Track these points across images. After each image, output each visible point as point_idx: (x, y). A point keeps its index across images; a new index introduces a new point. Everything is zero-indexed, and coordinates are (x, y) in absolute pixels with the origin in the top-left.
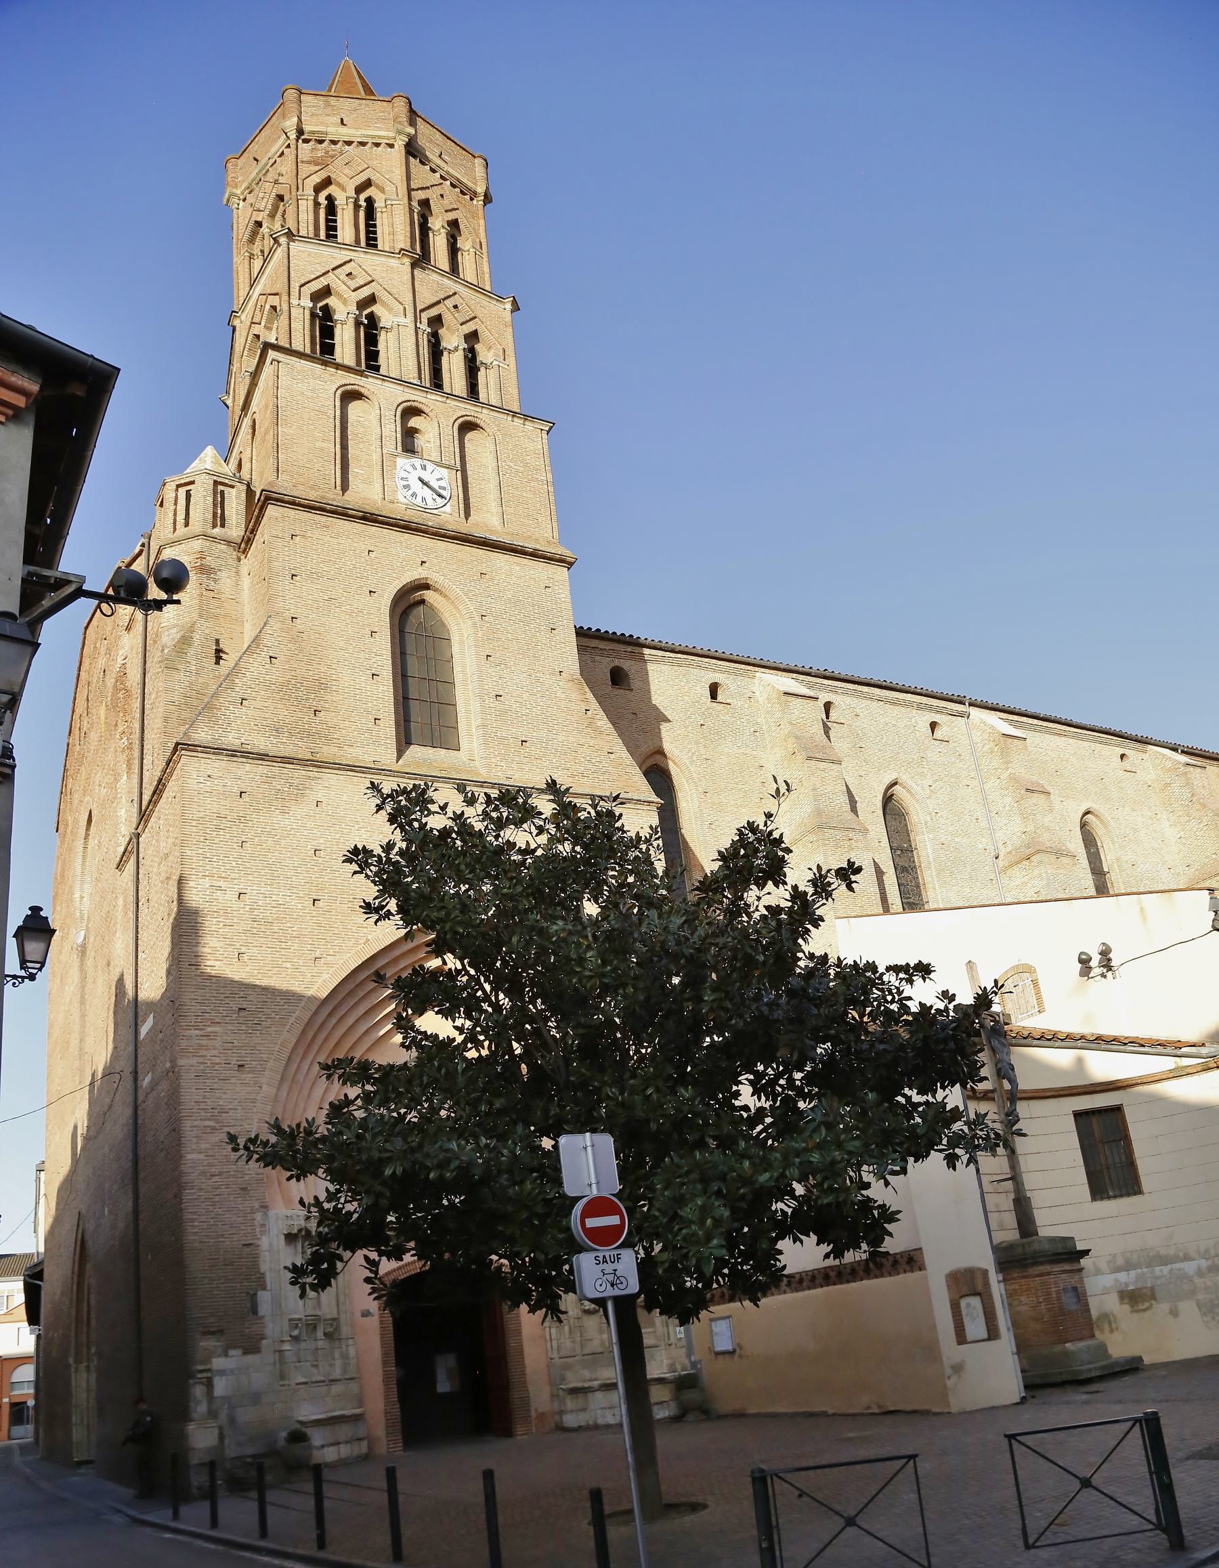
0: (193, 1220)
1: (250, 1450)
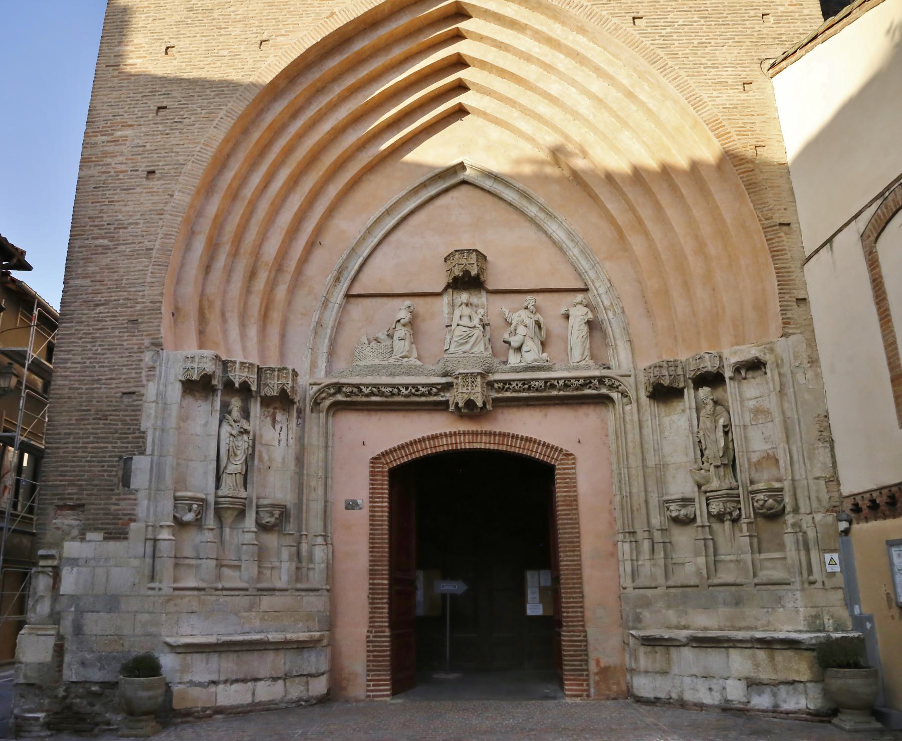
0: (66, 361)
1: (97, 675)
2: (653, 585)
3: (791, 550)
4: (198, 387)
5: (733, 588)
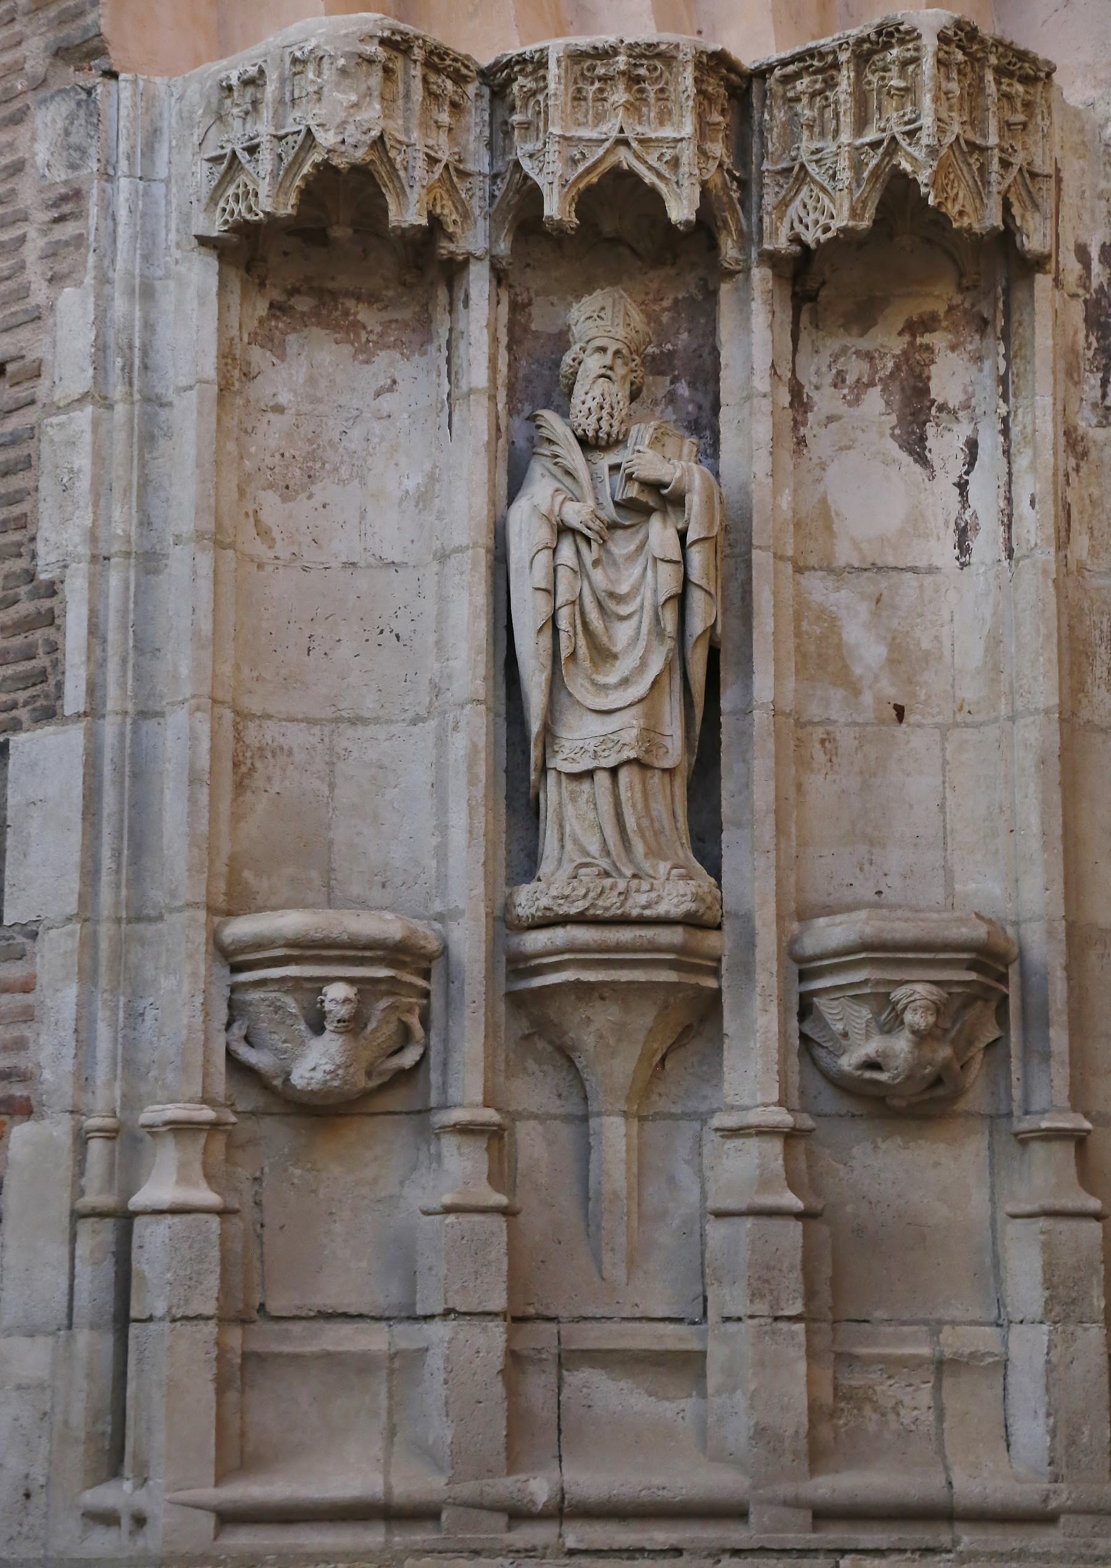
4: (322, 251)
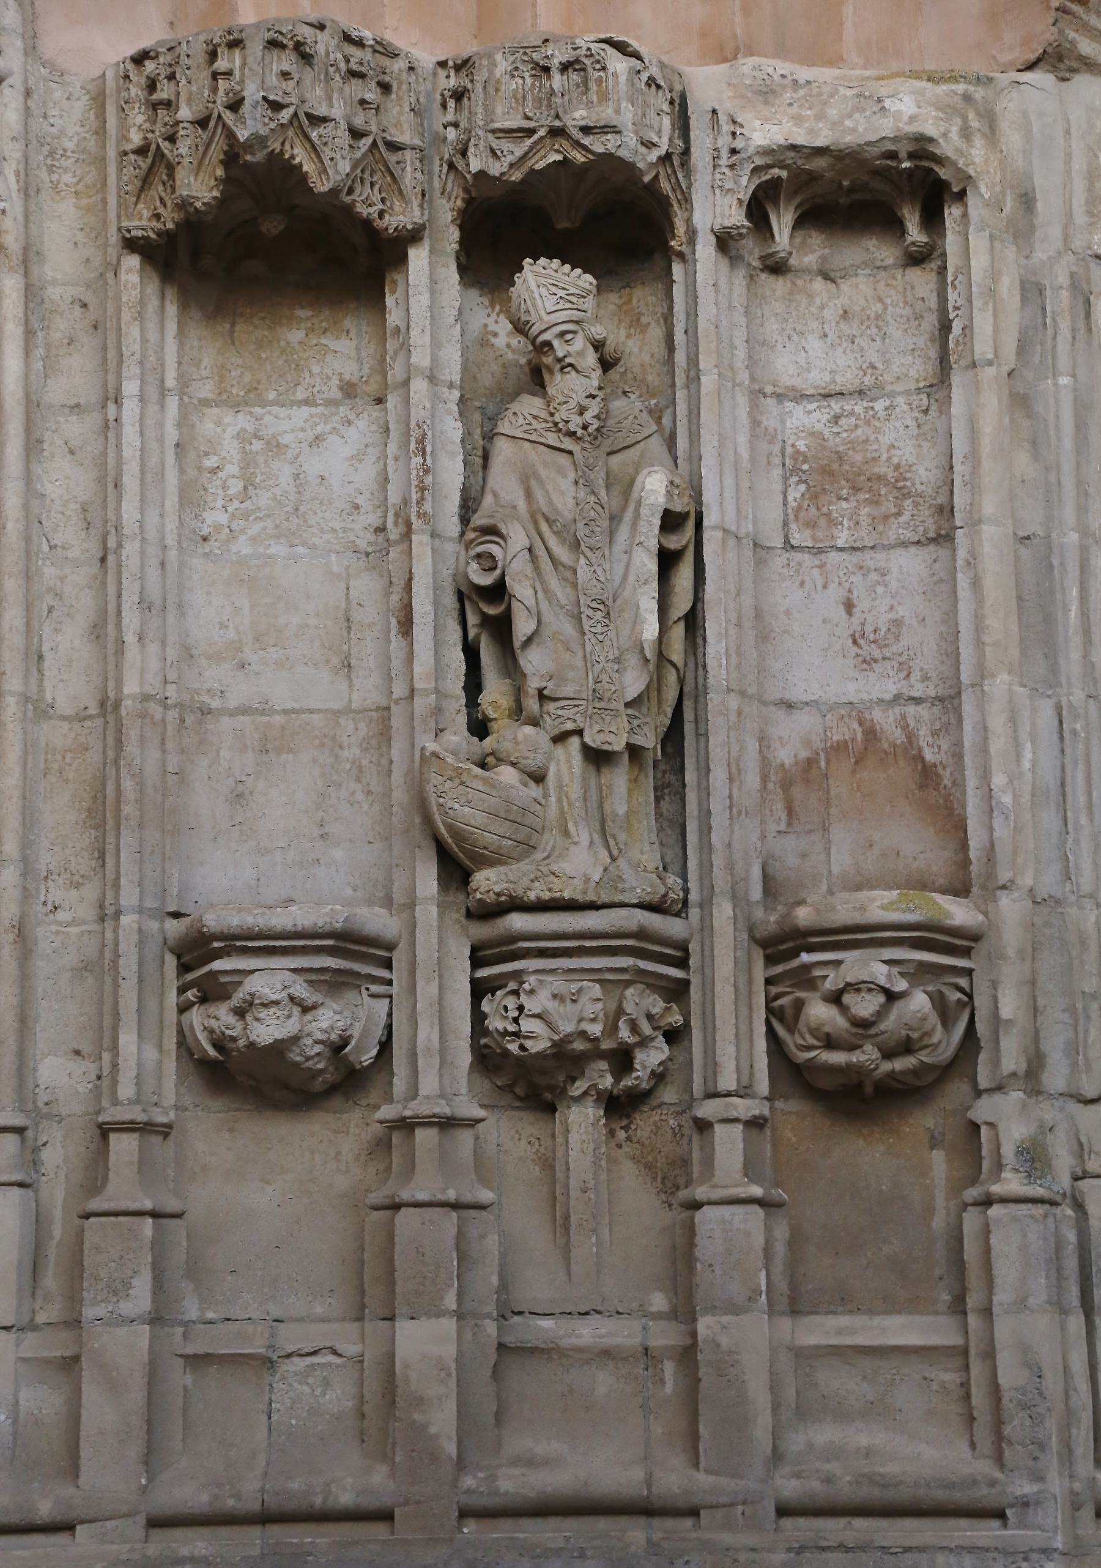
2: (45, 1510)
3: (1021, 1304)
5: (636, 1533)
